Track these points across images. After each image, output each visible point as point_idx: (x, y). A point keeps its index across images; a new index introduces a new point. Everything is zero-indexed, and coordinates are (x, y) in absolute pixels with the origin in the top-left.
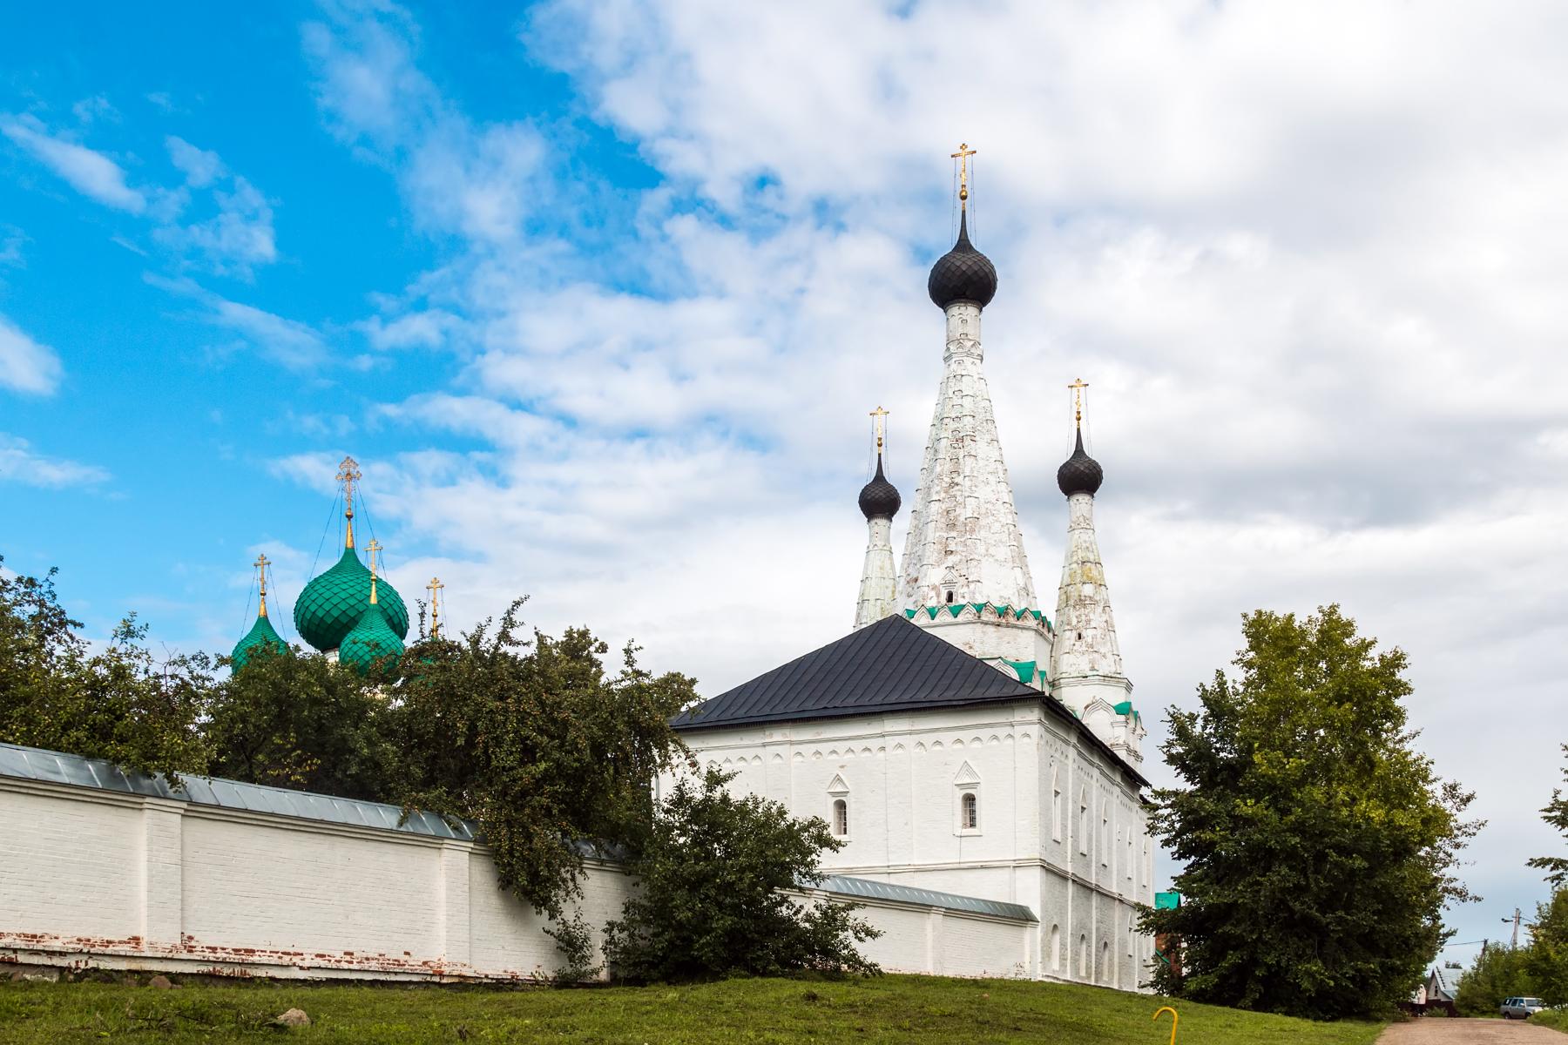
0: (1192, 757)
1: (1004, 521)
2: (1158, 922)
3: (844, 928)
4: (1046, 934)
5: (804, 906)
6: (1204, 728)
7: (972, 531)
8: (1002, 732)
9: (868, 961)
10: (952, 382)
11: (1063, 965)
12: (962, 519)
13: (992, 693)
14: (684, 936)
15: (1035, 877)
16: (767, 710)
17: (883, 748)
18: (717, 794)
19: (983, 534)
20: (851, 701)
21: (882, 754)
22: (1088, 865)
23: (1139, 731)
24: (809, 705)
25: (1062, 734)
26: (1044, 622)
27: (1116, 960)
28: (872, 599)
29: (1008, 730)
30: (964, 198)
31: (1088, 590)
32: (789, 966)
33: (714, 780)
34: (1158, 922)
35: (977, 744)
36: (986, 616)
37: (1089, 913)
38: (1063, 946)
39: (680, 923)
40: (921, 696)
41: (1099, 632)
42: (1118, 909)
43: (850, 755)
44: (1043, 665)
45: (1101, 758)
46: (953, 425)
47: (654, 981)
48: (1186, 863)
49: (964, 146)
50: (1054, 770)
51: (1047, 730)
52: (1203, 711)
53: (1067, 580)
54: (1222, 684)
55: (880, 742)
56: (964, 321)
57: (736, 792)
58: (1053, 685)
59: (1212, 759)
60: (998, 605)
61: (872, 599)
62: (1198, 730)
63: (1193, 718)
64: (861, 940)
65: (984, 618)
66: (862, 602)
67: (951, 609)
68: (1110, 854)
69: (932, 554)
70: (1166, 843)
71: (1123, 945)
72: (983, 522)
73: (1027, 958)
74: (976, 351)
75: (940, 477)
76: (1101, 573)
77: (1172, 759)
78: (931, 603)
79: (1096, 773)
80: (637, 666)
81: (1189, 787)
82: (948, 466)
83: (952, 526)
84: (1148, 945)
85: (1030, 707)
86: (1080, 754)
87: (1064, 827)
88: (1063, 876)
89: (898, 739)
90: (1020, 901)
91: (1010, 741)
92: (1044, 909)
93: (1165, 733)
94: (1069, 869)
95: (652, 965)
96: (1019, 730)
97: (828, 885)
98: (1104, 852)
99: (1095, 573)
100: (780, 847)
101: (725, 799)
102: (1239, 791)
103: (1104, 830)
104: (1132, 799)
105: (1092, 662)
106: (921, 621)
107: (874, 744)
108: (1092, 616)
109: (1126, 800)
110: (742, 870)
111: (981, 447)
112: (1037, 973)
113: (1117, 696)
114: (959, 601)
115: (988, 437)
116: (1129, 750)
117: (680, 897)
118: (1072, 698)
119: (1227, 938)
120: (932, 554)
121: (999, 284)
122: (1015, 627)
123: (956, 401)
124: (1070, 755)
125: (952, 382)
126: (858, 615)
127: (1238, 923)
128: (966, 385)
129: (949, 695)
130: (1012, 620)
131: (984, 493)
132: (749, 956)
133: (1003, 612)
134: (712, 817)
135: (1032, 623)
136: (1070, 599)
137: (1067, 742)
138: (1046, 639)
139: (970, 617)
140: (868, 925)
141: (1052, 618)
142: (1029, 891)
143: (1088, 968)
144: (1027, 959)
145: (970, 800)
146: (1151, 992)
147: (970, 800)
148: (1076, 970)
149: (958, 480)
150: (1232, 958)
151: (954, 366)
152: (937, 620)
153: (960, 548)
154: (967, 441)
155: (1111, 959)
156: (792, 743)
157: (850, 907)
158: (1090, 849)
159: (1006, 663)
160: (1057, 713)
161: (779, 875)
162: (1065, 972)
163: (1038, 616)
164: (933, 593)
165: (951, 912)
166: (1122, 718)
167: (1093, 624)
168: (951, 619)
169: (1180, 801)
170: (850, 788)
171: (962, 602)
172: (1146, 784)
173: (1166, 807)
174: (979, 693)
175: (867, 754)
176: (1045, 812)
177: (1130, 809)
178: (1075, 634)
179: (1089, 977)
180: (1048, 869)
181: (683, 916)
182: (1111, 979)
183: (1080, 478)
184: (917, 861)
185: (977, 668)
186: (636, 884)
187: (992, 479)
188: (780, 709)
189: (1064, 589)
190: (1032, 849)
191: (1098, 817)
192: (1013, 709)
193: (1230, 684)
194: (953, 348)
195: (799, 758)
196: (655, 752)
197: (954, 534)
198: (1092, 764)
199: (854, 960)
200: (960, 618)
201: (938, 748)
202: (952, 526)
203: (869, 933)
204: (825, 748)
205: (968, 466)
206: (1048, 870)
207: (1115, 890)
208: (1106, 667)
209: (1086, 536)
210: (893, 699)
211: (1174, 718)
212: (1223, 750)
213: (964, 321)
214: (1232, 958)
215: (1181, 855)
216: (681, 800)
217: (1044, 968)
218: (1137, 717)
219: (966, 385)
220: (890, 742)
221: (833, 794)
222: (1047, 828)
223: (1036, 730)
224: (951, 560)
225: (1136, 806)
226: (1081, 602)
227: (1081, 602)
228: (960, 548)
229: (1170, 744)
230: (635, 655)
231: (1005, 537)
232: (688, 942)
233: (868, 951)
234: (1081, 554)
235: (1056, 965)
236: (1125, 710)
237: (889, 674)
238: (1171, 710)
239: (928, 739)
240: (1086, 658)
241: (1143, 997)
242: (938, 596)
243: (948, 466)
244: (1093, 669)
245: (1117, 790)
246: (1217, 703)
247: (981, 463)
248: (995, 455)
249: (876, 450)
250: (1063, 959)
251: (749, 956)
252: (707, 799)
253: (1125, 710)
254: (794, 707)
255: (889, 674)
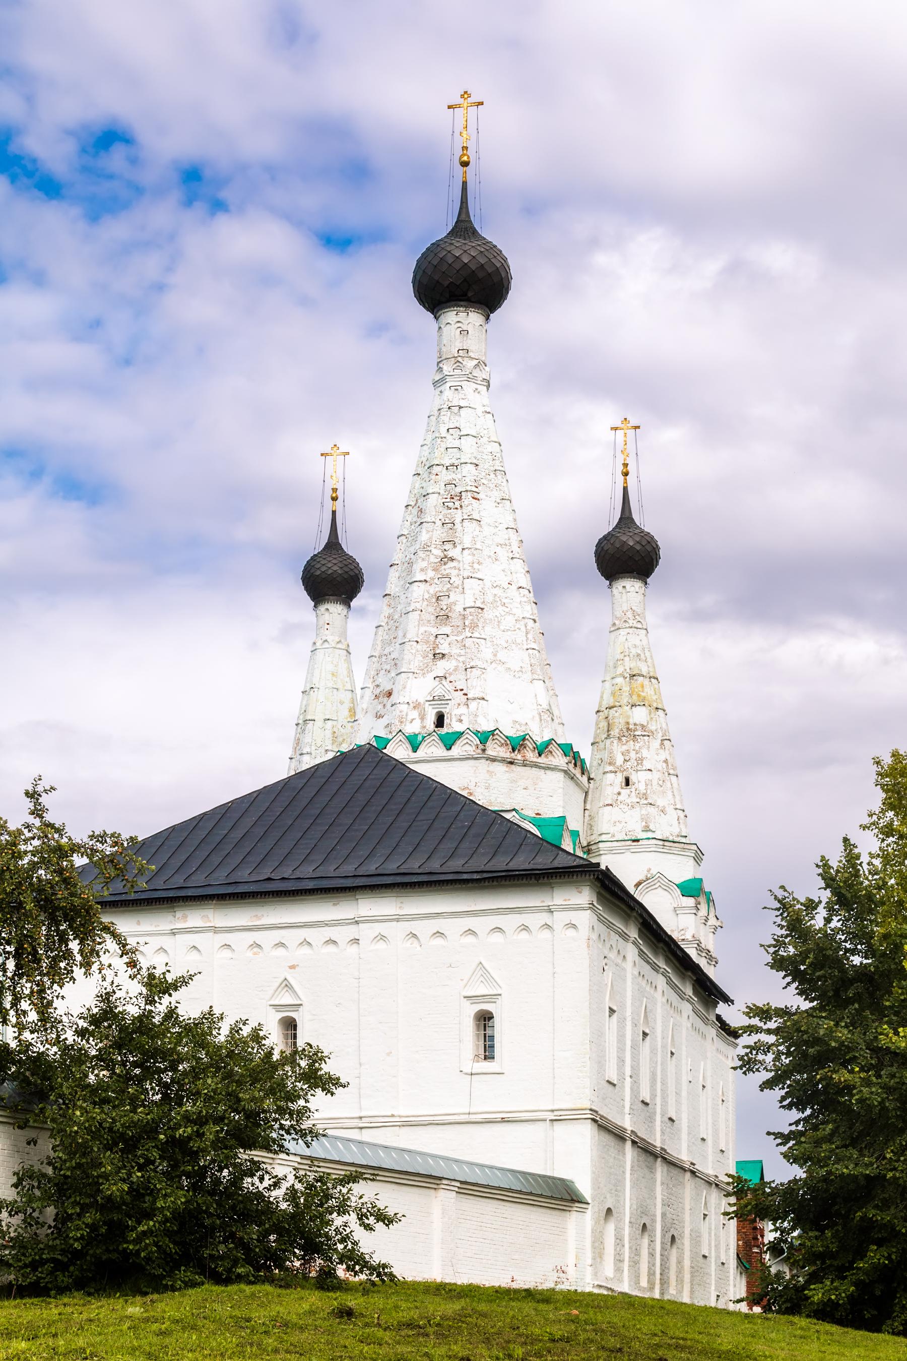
0: (807, 960)
1: (519, 613)
2: (752, 1202)
3: (342, 1209)
4: (597, 1222)
5: (279, 1174)
6: (828, 920)
7: (474, 626)
8: (535, 920)
9: (376, 1259)
10: (446, 416)
11: (618, 1270)
12: (459, 608)
13: (521, 862)
14: (117, 1217)
15: (585, 1134)
16: (179, 881)
17: (356, 941)
18: (161, 1007)
19: (488, 631)
20: (308, 870)
21: (354, 948)
22: (651, 1119)
23: (712, 921)
24: (244, 874)
25: (619, 924)
26: (576, 759)
27: (687, 1263)
28: (319, 718)
29: (544, 918)
30: (465, 164)
31: (639, 715)
32: (263, 1266)
33: (158, 986)
34: (752, 1202)
35: (497, 937)
36: (493, 749)
37: (652, 1190)
38: (619, 1240)
39: (109, 1199)
40: (414, 865)
41: (655, 776)
42: (689, 1184)
43: (305, 950)
44: (575, 823)
45: (668, 961)
46: (446, 476)
47: (62, 1291)
48: (795, 1115)
49: (465, 95)
50: (609, 974)
51: (601, 920)
52: (826, 895)
53: (608, 700)
54: (852, 858)
55: (352, 931)
56: (464, 332)
57: (189, 1005)
58: (589, 852)
59: (838, 963)
60: (510, 732)
61: (319, 718)
62: (818, 922)
63: (811, 905)
64: (368, 1228)
65: (490, 752)
66: (304, 723)
67: (441, 738)
68: (678, 1103)
69: (413, 657)
70: (768, 1085)
71: (696, 1239)
72: (488, 614)
73: (572, 1258)
74: (480, 374)
75: (426, 548)
76: (657, 692)
77: (779, 963)
78: (412, 728)
79: (661, 981)
80: (49, 817)
81: (806, 1005)
82: (439, 533)
83: (444, 617)
84: (724, 1238)
85: (577, 884)
86: (641, 954)
87: (621, 1061)
88: (618, 1135)
89: (378, 928)
90: (560, 1172)
91: (546, 933)
92: (596, 1185)
93: (771, 927)
94: (627, 1123)
95: (59, 1266)
96: (561, 918)
97: (318, 1149)
98: (672, 1100)
99: (649, 691)
100: (258, 1086)
101: (171, 1014)
102: (880, 1013)
103: (671, 1064)
104: (705, 1021)
105: (645, 819)
106: (399, 752)
107: (343, 934)
108: (645, 753)
109: (699, 1023)
110: (201, 1121)
111: (486, 508)
112: (584, 1281)
113: (681, 869)
114: (453, 725)
115: (497, 495)
116: (700, 949)
117: (108, 1162)
118: (627, 869)
119: (868, 1225)
120: (413, 657)
121: (513, 283)
122: (536, 765)
123: (451, 441)
124: (630, 953)
125: (446, 416)
126: (298, 742)
127: (885, 1205)
128: (465, 420)
129: (457, 864)
130: (531, 756)
131: (492, 572)
132: (206, 1253)
133: (518, 744)
134: (138, 1041)
135: (559, 760)
136: (608, 730)
137: (624, 937)
138: (578, 784)
139: (470, 750)
140: (380, 1205)
141: (586, 754)
142: (574, 1156)
143: (651, 1274)
144: (571, 1261)
145: (485, 1019)
146: (743, 1307)
147: (485, 1019)
148: (636, 1278)
149: (453, 553)
150: (875, 1256)
151: (448, 394)
152: (421, 753)
153: (455, 650)
154: (467, 499)
155: (680, 1262)
156: (216, 930)
157: (353, 1178)
158: (653, 1096)
159: (524, 818)
160: (613, 895)
161: (251, 1133)
162: (621, 1281)
163: (568, 750)
164: (415, 714)
165: (469, 1188)
166: (691, 902)
167: (647, 765)
168: (441, 752)
169: (792, 1029)
170: (305, 1000)
171: (458, 727)
172: (727, 1000)
173: (769, 1032)
174: (500, 863)
175: (331, 948)
176: (597, 1038)
177: (704, 1037)
178: (620, 779)
179: (651, 1288)
180: (603, 1126)
181: (115, 1189)
182: (680, 1292)
183: (627, 556)
184: (404, 1111)
185: (494, 826)
186: (32, 1142)
187: (503, 554)
188: (199, 879)
189: (604, 712)
190: (580, 1094)
191: (664, 1047)
192: (551, 887)
193: (865, 859)
194: (447, 368)
195: (227, 953)
196: (74, 945)
197: (446, 630)
198: (655, 968)
199: (355, 1260)
200: (456, 751)
201: (439, 941)
202: (444, 617)
203: (385, 1219)
204: (267, 938)
205: (467, 534)
206: (600, 1127)
207: (683, 1155)
208: (667, 827)
209: (636, 639)
210: (372, 868)
211: (784, 906)
212: (854, 952)
213: (464, 332)
214: (875, 1256)
215: (799, 1105)
216: (105, 1015)
217: (595, 1274)
218: (710, 901)
219: (465, 420)
220: (367, 931)
221: (277, 1007)
222: (600, 1063)
223: (585, 919)
224: (442, 667)
225: (712, 1032)
226: (630, 732)
227: (630, 732)
228: (455, 650)
229: (779, 943)
230: (44, 800)
231: (520, 636)
232: (117, 1231)
233: (375, 1244)
234: (629, 665)
235: (609, 1270)
236: (692, 889)
237: (360, 829)
238: (780, 894)
239: (425, 928)
240: (637, 813)
241: (738, 1314)
242: (422, 718)
243: (439, 533)
244: (647, 829)
245: (687, 1008)
246: (845, 888)
247: (487, 531)
248: (508, 520)
249: (329, 505)
250: (619, 1260)
251: (206, 1253)
252: (146, 1016)
253: (692, 889)
254: (221, 876)
255: (360, 829)
